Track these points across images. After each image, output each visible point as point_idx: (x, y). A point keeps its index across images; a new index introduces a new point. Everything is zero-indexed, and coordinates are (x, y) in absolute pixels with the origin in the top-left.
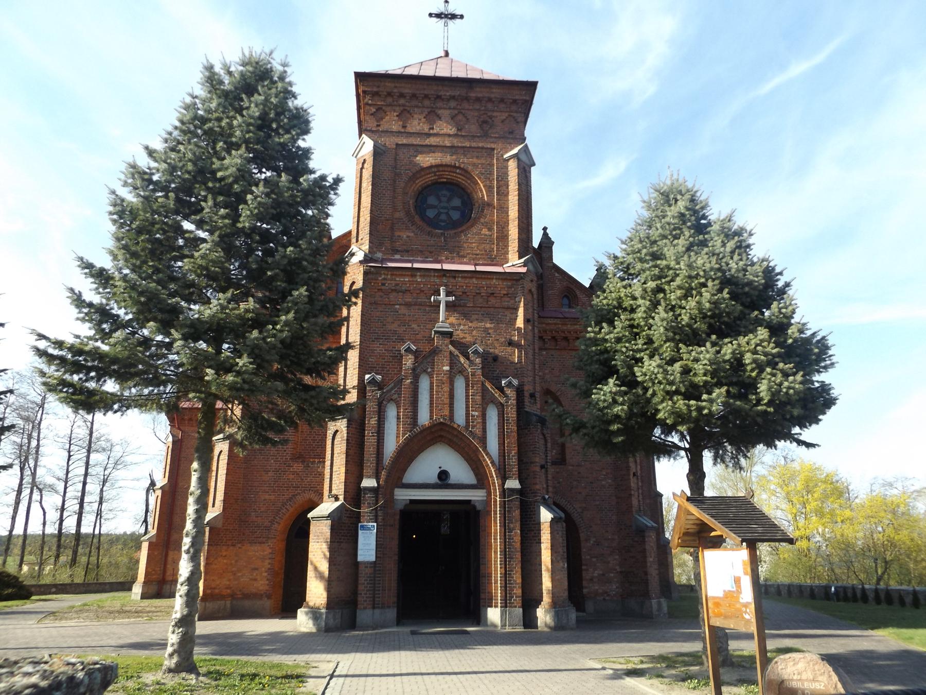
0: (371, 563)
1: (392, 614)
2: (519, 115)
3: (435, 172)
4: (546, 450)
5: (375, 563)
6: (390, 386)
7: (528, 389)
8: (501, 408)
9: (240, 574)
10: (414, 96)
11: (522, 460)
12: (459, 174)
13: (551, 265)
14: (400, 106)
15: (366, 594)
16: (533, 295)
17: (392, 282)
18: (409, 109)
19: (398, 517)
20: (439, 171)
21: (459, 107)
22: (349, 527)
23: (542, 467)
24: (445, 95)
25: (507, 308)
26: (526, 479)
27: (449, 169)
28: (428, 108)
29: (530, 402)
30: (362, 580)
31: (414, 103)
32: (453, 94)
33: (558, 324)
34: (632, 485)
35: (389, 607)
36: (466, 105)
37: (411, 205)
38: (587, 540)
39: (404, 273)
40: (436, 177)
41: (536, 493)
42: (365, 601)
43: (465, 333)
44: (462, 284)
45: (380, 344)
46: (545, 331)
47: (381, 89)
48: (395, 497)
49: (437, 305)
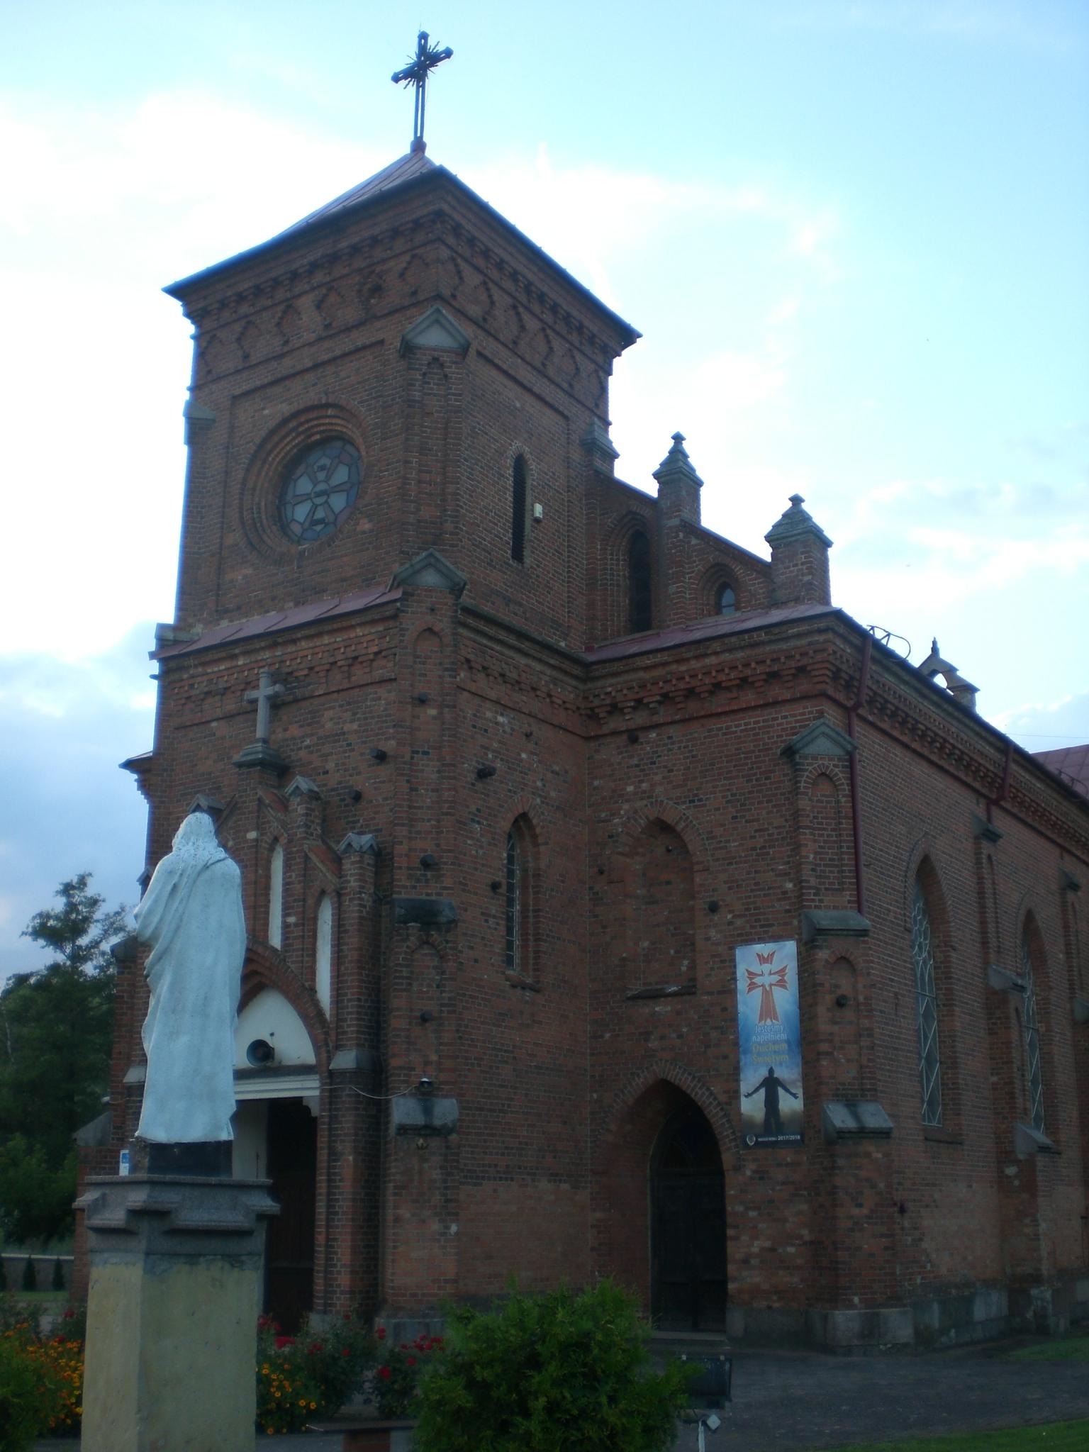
20: (302, 424)
38: (738, 1168)
40: (302, 437)
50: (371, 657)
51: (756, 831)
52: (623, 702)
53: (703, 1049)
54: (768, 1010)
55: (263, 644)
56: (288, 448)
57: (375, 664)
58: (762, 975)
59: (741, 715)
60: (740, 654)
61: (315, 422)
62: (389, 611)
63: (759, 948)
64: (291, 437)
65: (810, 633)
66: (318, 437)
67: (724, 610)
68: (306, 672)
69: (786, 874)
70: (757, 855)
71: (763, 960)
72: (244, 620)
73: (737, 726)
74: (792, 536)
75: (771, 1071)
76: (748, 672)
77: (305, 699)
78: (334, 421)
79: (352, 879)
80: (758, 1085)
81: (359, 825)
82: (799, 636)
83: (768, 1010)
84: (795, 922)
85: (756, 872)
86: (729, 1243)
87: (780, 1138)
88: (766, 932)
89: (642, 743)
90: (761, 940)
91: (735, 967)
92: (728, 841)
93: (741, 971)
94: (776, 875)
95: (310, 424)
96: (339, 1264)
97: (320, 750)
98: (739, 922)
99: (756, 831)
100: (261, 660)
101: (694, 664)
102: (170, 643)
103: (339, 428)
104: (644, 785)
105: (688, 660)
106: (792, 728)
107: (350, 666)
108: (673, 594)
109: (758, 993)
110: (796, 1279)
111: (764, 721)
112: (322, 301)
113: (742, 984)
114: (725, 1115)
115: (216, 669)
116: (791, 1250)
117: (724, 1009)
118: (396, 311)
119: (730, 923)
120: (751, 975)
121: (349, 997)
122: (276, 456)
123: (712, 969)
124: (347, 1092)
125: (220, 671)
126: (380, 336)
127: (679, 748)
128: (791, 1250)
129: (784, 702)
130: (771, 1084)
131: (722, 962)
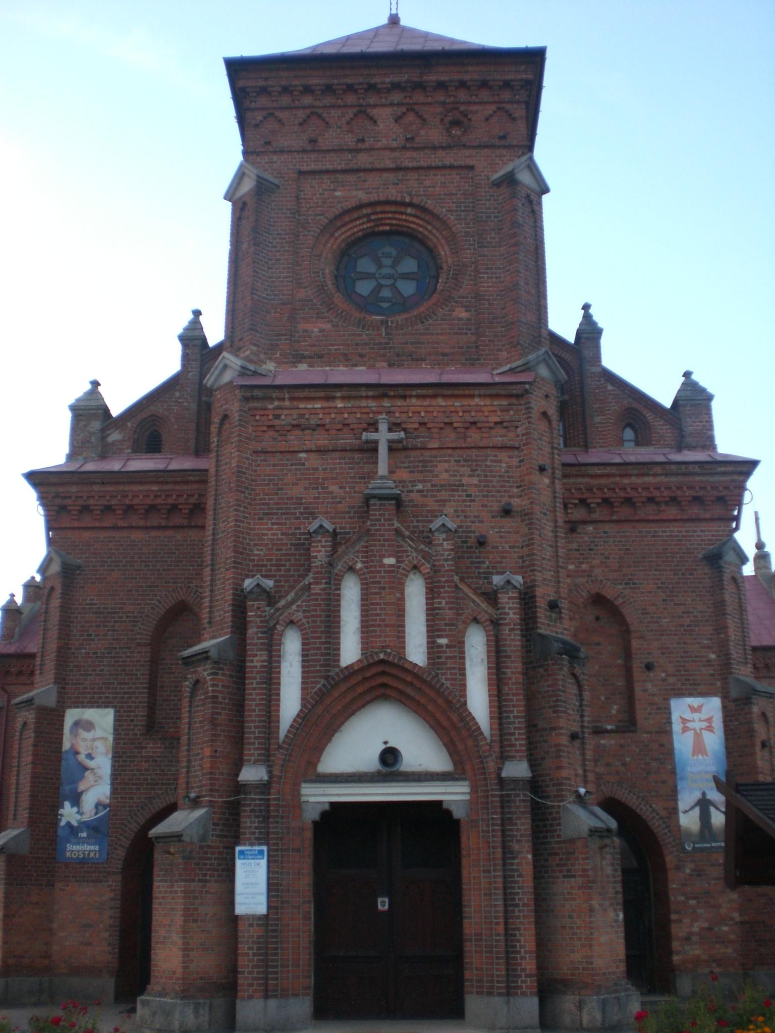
0: (260, 918)
1: (302, 1006)
2: (515, 106)
3: (368, 215)
4: (581, 705)
5: (266, 917)
6: (289, 598)
7: (544, 593)
8: (494, 626)
9: (62, 934)
10: (328, 89)
11: (535, 726)
12: (410, 215)
13: (598, 370)
14: (305, 107)
15: (250, 973)
16: (549, 421)
17: (292, 412)
18: (320, 111)
19: (309, 834)
21: (408, 101)
22: (220, 853)
23: (574, 737)
24: (383, 83)
25: (502, 448)
26: (543, 759)
27: (393, 209)
28: (351, 106)
29: (550, 617)
30: (243, 948)
31: (328, 100)
32: (396, 80)
33: (614, 475)
34: (760, 763)
35: (295, 995)
36: (418, 97)
37: (328, 276)
39: (312, 395)
40: (372, 224)
41: (561, 784)
42: (249, 985)
43: (426, 496)
44: (418, 409)
45: (273, 524)
46: (590, 490)
47: (270, 83)
48: (304, 799)
49: (372, 449)
50: (492, 425)
51: (683, 613)
52: (569, 498)
53: (645, 775)
54: (699, 748)
55: (371, 394)
56: (355, 230)
57: (494, 432)
58: (693, 721)
59: (667, 524)
60: (674, 479)
61: (390, 215)
62: (516, 390)
63: (690, 700)
64: (361, 221)
65: (733, 473)
66: (388, 228)
67: (626, 444)
68: (416, 426)
69: (709, 647)
70: (685, 630)
71: (694, 710)
72: (327, 368)
73: (663, 532)
74: (698, 400)
75: (704, 794)
76: (679, 493)
77: (415, 448)
78: (411, 219)
79: (511, 612)
80: (693, 804)
81: (485, 566)
82: (724, 474)
83: (699, 748)
84: (719, 684)
85: (685, 643)
86: (673, 925)
87: (714, 844)
88: (694, 689)
89: (580, 533)
90: (691, 695)
91: (670, 713)
92: (660, 618)
93: (675, 717)
94: (701, 648)
95: (383, 216)
96: (523, 950)
97: (436, 496)
98: (672, 680)
99: (683, 613)
100: (364, 407)
101: (634, 480)
102: (249, 373)
103: (414, 226)
104: (584, 566)
105: (630, 476)
106: (709, 540)
107: (467, 428)
108: (598, 423)
109: (690, 734)
110: (730, 951)
111: (686, 531)
112: (400, 117)
113: (676, 727)
114: (667, 827)
115: (310, 406)
116: (725, 928)
117: (661, 745)
118: (486, 147)
119: (664, 680)
120: (684, 721)
121: (516, 714)
122: (342, 234)
123: (650, 714)
124: (522, 798)
125: (314, 408)
126: (470, 162)
127: (614, 541)
128: (725, 928)
129: (705, 520)
130: (704, 804)
131: (658, 709)
